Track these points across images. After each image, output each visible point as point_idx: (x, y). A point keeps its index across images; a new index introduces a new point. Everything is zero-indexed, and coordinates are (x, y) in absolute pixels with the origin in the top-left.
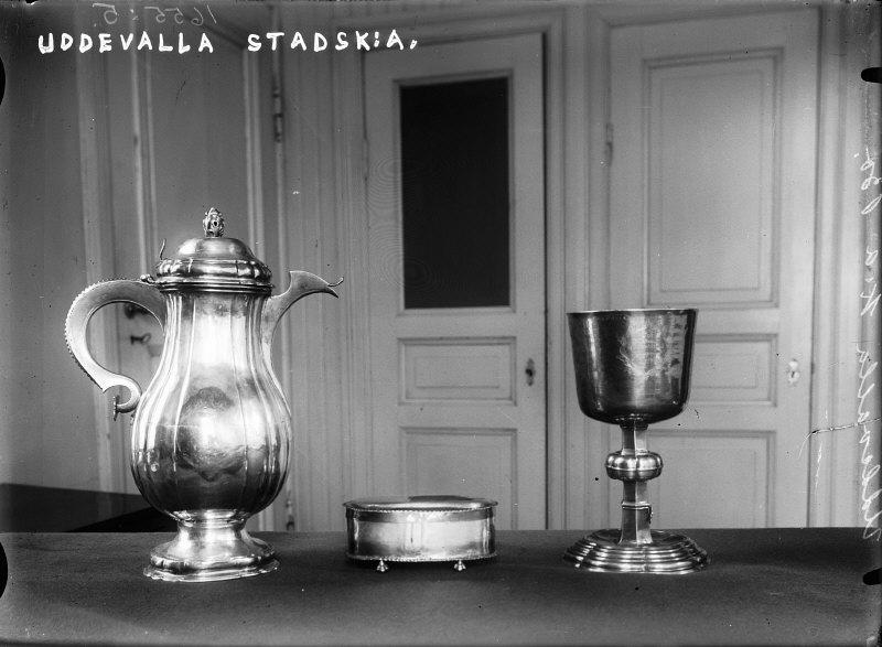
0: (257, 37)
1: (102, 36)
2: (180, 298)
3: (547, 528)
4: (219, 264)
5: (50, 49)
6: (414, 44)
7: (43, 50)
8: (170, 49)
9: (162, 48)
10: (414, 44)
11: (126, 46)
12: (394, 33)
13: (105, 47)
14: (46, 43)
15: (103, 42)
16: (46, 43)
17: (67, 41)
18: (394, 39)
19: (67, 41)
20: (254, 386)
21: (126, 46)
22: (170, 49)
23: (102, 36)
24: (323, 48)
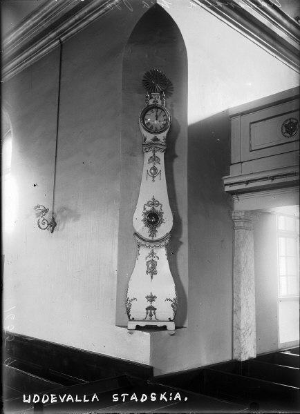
0: (155, 394)
1: (52, 395)
2: (295, 115)
3: (226, 185)
4: (109, 9)
5: (29, 401)
6: (186, 399)
7: (25, 401)
8: (80, 401)
9: (77, 400)
10: (186, 399)
11: (62, 401)
12: (95, 395)
13: (153, 399)
14: (27, 399)
15: (52, 399)
16: (27, 399)
17: (144, 398)
18: (178, 396)
19: (144, 398)
20: (226, 185)
21: (62, 401)
22: (80, 401)
23: (52, 395)
24: (145, 400)
